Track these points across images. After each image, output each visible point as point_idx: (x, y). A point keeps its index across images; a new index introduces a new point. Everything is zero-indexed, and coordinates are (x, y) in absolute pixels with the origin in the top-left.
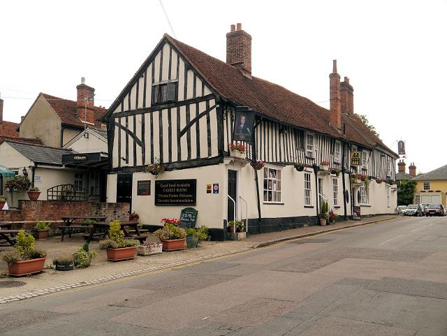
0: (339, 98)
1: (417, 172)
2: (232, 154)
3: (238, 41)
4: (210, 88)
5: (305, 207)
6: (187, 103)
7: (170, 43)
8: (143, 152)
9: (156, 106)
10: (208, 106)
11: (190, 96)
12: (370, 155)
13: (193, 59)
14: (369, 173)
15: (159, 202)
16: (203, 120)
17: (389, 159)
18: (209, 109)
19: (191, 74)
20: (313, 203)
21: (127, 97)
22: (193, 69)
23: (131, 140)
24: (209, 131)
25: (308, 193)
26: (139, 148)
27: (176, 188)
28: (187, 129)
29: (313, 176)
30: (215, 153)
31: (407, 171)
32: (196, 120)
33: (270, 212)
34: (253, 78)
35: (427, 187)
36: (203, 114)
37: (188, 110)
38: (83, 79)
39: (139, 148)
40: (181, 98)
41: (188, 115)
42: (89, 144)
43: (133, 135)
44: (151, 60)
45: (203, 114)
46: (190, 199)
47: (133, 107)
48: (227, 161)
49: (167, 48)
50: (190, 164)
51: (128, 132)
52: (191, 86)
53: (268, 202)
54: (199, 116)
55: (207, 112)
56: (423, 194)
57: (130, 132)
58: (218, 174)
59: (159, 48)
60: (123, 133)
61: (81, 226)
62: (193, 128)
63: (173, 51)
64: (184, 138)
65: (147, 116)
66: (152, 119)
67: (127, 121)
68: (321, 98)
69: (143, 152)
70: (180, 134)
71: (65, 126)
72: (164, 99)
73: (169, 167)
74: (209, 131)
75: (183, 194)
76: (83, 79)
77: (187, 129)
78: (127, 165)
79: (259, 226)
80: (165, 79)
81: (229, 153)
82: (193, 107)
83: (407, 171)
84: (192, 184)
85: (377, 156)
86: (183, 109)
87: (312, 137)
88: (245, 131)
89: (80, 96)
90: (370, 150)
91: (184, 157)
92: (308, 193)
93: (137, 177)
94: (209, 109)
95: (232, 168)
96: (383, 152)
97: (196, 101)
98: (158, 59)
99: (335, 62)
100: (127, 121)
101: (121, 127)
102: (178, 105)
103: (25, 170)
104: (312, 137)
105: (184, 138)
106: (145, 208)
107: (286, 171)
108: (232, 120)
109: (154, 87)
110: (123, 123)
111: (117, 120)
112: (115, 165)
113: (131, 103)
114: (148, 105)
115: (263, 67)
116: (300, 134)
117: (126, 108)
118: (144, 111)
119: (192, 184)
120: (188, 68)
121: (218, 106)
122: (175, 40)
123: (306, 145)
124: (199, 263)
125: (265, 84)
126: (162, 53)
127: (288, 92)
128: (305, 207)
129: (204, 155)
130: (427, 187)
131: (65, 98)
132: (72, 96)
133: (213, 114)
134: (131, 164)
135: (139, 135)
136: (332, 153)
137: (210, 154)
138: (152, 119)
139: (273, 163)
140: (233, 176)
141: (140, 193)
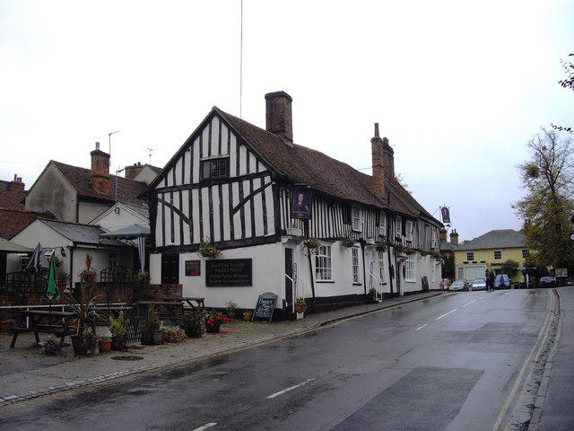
0: (382, 164)
1: (461, 240)
2: (288, 233)
3: (278, 105)
4: (265, 164)
5: (354, 284)
6: (240, 179)
7: (219, 117)
8: (192, 230)
9: (205, 183)
10: (263, 182)
11: (243, 172)
12: (414, 225)
13: (237, 127)
14: (414, 245)
15: (211, 283)
16: (258, 198)
17: (433, 228)
18: (264, 186)
19: (243, 150)
20: (361, 280)
21: (172, 171)
22: (245, 144)
23: (177, 217)
24: (264, 208)
25: (355, 268)
26: (186, 226)
27: (222, 268)
28: (241, 206)
29: (360, 250)
30: (271, 232)
31: (449, 240)
32: (251, 197)
33: (323, 291)
34: (295, 145)
35: (470, 257)
36: (257, 191)
37: (241, 186)
38: (98, 144)
39: (186, 226)
40: (233, 174)
41: (241, 192)
42: (122, 221)
43: (180, 212)
44: (198, 133)
45: (257, 191)
46: (246, 278)
47: (179, 183)
48: (284, 240)
49: (215, 122)
50: (244, 243)
51: (173, 209)
52: (243, 162)
53: (324, 280)
54: (253, 193)
55: (262, 190)
56: (466, 265)
57: (169, 205)
58: (276, 251)
59: (208, 121)
60: (168, 210)
61: (48, 312)
62: (247, 205)
63: (231, 134)
64: (237, 216)
65: (195, 192)
66: (200, 195)
67: (172, 197)
68: (363, 162)
69: (192, 230)
70: (232, 212)
71: (81, 199)
72: (217, 173)
73: (223, 245)
74: (264, 208)
75: (240, 274)
76: (98, 144)
77: (241, 206)
78: (172, 244)
79: (316, 306)
80: (215, 154)
81: (285, 231)
82: (246, 184)
83: (449, 240)
84: (247, 263)
85: (421, 225)
86: (235, 185)
87: (358, 210)
88: (303, 209)
89: (94, 163)
90: (414, 220)
91: (238, 236)
92: (355, 268)
93: (184, 258)
94: (264, 186)
95: (288, 247)
96: (426, 221)
97: (250, 177)
98: (206, 133)
99: (377, 125)
100: (172, 197)
101: (165, 203)
102: (230, 181)
103: (63, 250)
104: (358, 210)
105: (237, 216)
106: (193, 287)
107: (336, 246)
108: (287, 197)
109: (202, 163)
110: (167, 197)
111: (160, 196)
112: (159, 243)
113: (173, 179)
114: (196, 180)
115: (303, 135)
116: (347, 208)
117: (170, 184)
118: (191, 187)
119: (247, 263)
120: (240, 142)
121: (274, 183)
122: (225, 114)
123: (353, 217)
124: (69, 394)
125: (306, 151)
126: (211, 126)
127: (329, 158)
128: (354, 284)
129: (260, 232)
130: (470, 257)
131: (75, 165)
132: (86, 163)
133: (269, 191)
134: (177, 242)
135: (186, 212)
136: (378, 225)
137: (266, 232)
138: (200, 195)
139: (323, 239)
140: (289, 253)
141: (188, 273)
